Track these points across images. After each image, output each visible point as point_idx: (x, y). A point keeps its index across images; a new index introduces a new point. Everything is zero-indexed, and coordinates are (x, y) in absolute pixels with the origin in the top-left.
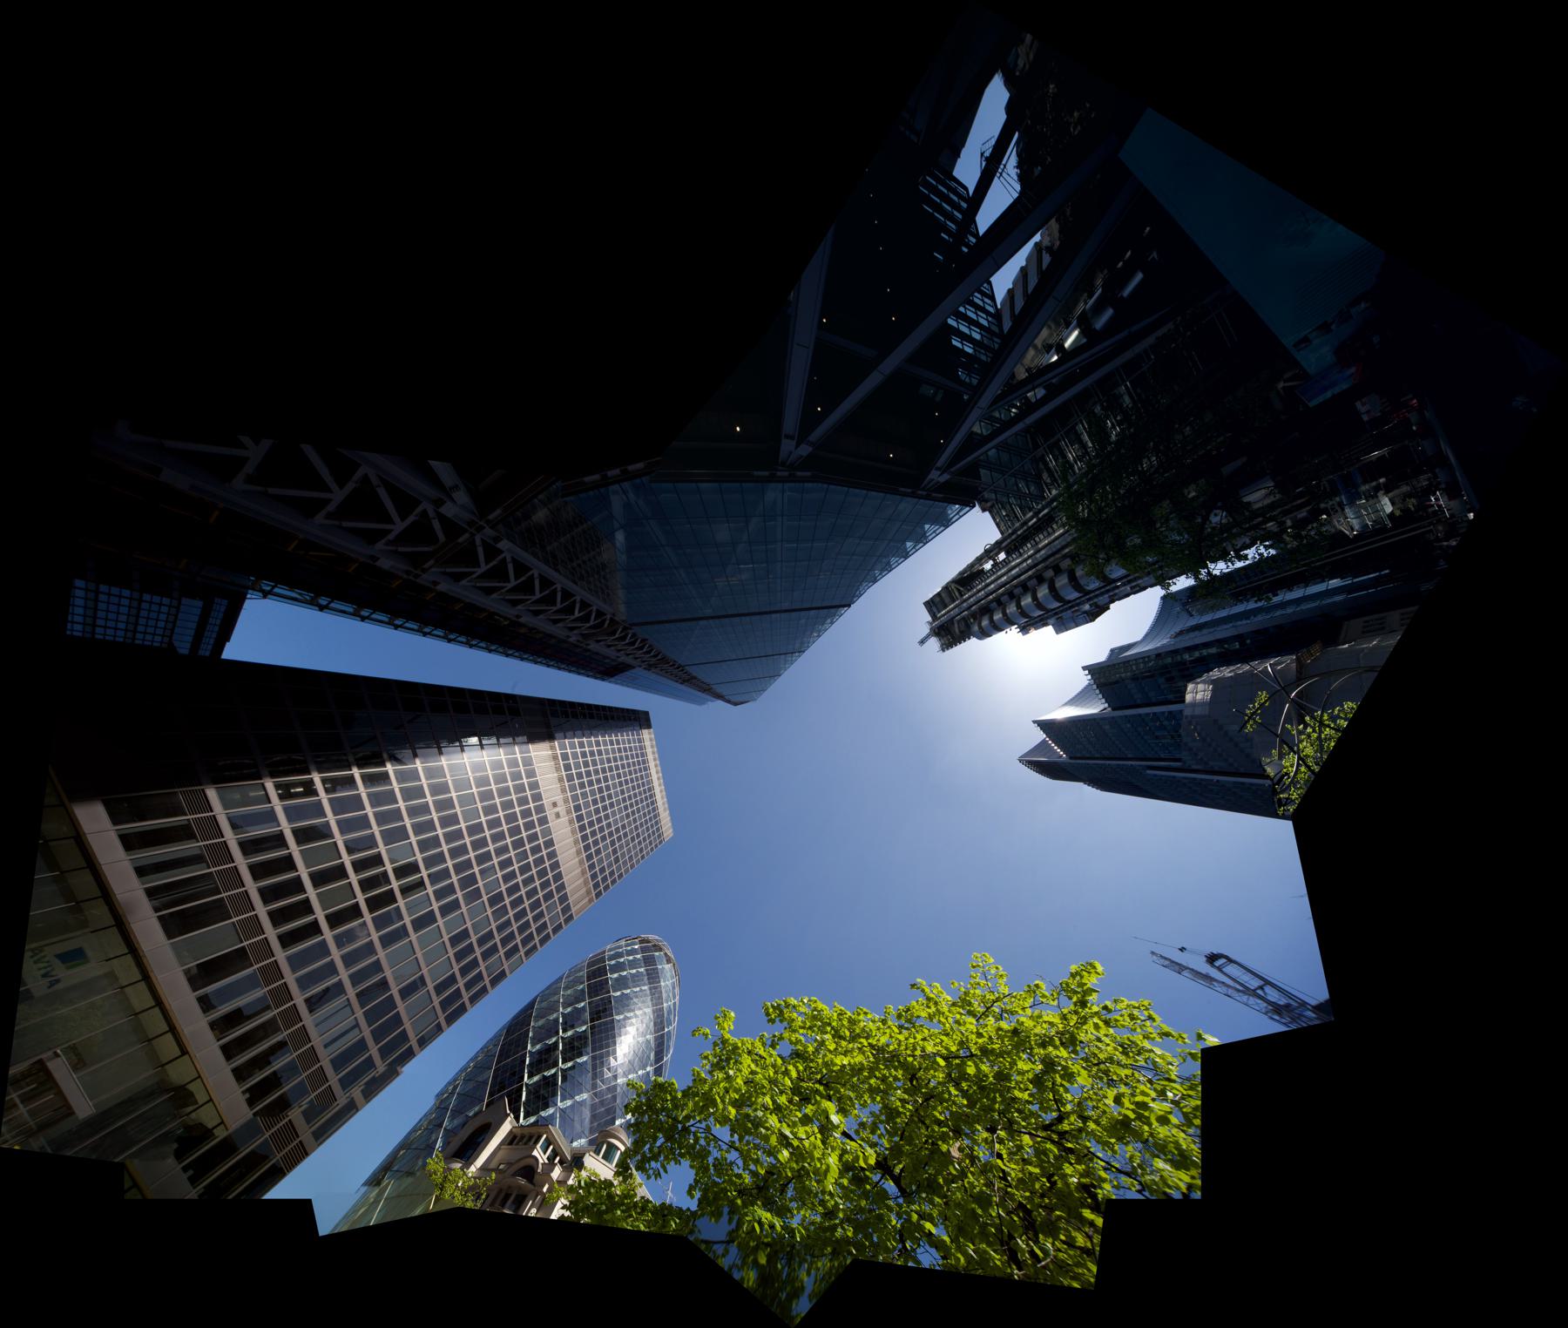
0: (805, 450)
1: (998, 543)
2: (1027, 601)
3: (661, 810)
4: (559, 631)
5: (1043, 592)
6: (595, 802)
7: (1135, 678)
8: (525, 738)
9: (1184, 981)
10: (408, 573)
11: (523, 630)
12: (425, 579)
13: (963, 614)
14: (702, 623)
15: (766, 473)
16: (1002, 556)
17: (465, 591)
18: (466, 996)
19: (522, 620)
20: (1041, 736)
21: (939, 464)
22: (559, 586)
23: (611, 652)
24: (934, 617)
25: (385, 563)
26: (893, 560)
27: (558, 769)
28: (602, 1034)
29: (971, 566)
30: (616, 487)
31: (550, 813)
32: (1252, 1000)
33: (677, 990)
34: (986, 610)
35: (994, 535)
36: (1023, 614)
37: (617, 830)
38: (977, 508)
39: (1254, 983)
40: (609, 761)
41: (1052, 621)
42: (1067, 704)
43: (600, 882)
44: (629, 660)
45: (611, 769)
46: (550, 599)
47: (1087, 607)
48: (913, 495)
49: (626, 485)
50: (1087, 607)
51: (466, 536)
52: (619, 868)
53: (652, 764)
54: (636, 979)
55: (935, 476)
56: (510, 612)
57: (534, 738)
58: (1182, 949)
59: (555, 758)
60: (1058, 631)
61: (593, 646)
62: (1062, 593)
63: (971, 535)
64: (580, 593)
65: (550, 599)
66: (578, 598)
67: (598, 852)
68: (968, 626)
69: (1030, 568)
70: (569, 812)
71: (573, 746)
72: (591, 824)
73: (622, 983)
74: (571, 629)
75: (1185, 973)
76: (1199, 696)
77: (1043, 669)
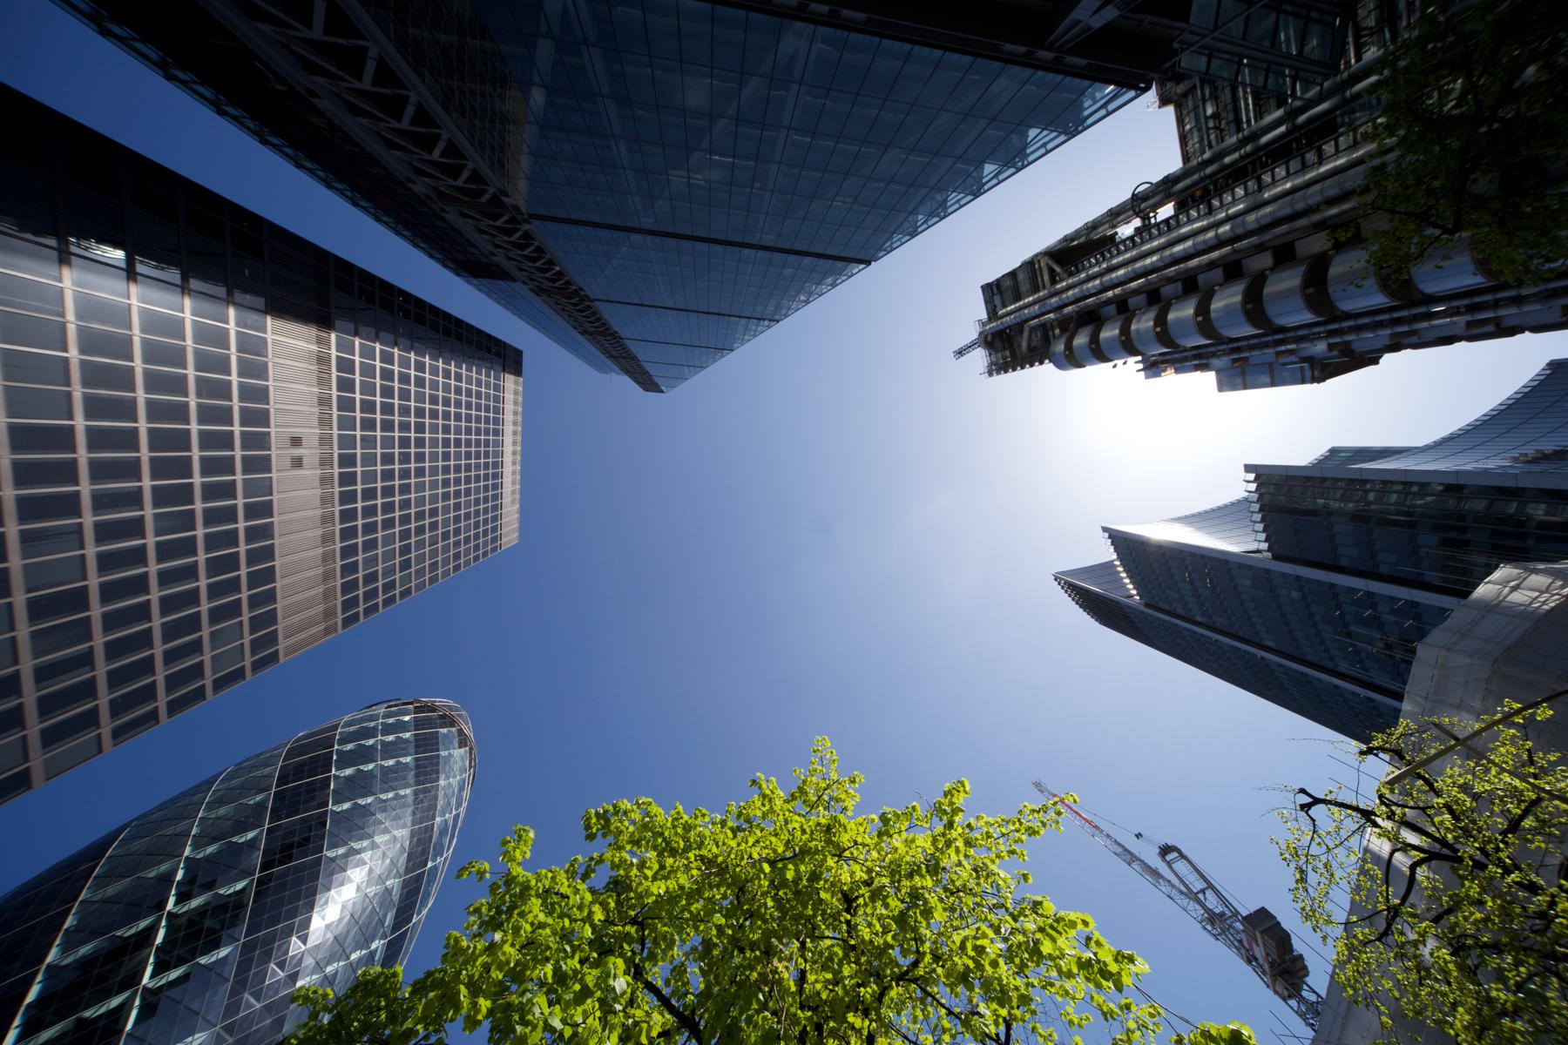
1: (1169, 181)
2: (1183, 312)
3: (507, 500)
4: (395, 162)
5: (1227, 300)
7: (1361, 518)
8: (260, 302)
9: (1132, 874)
14: (635, 237)
16: (1166, 211)
18: (162, 700)
20: (1108, 554)
22: (470, 166)
23: (483, 242)
26: (954, 197)
27: (323, 381)
28: (293, 872)
29: (1094, 225)
31: (279, 454)
32: (1193, 905)
33: (466, 793)
34: (1091, 318)
35: (1169, 161)
36: (1164, 335)
37: (420, 516)
38: (1151, 96)
39: (1198, 885)
41: (1222, 362)
42: (1180, 520)
43: (358, 595)
44: (510, 267)
46: (395, 107)
47: (1320, 347)
48: (1028, 62)
50: (1320, 347)
53: (509, 429)
54: (390, 778)
57: (282, 307)
58: (1138, 836)
59: (323, 360)
60: (1222, 386)
61: (452, 216)
62: (1271, 310)
63: (1127, 149)
66: (470, 166)
68: (1047, 341)
69: (1220, 243)
70: (325, 462)
71: (372, 356)
73: (361, 785)
75: (1136, 865)
76: (1518, 597)
77: (1176, 448)
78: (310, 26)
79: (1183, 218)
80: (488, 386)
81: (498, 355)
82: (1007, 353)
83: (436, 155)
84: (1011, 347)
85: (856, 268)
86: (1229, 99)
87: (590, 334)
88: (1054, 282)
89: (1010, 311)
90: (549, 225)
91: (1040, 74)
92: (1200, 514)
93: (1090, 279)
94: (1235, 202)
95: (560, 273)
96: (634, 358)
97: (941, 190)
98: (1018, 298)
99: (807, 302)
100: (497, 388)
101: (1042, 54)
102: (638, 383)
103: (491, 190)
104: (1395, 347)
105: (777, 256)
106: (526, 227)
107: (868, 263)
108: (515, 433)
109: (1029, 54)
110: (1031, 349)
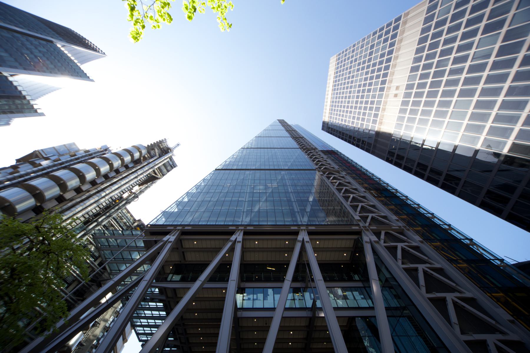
0: (233, 238)
4: (349, 179)
6: (369, 91)
10: (408, 230)
11: (366, 185)
12: (401, 224)
13: (152, 160)
14: (287, 168)
15: (248, 228)
17: (384, 211)
19: (364, 190)
21: (170, 244)
22: (341, 194)
23: (329, 161)
24: (171, 158)
25: (417, 238)
26: (195, 191)
30: (304, 223)
40: (351, 112)
43: (391, 32)
44: (322, 155)
45: (352, 107)
46: (347, 191)
49: (300, 223)
51: (371, 228)
52: (373, 40)
55: (172, 238)
56: (368, 195)
57: (388, 137)
61: (336, 167)
63: (150, 206)
64: (333, 189)
65: (347, 191)
66: (341, 194)
67: (382, 56)
68: (149, 152)
69: (103, 190)
72: (378, 77)
74: (343, 177)
78: (402, 247)
79: (119, 195)
80: (334, 118)
81: (329, 128)
82: (162, 147)
83: (352, 196)
84: (161, 149)
85: (220, 168)
86: (121, 224)
87: (300, 137)
88: (154, 171)
89: (165, 159)
90: (311, 168)
91: (179, 223)
92: (52, 91)
93: (142, 174)
94: (104, 202)
95: (314, 161)
96: (287, 131)
97: (199, 192)
98: (164, 165)
99: (233, 155)
100: (331, 117)
101: (180, 228)
102: (286, 122)
103: (325, 175)
104: (13, 167)
105: (244, 168)
106: (317, 167)
107: (216, 170)
108: (327, 102)
109: (184, 227)
110: (153, 149)
